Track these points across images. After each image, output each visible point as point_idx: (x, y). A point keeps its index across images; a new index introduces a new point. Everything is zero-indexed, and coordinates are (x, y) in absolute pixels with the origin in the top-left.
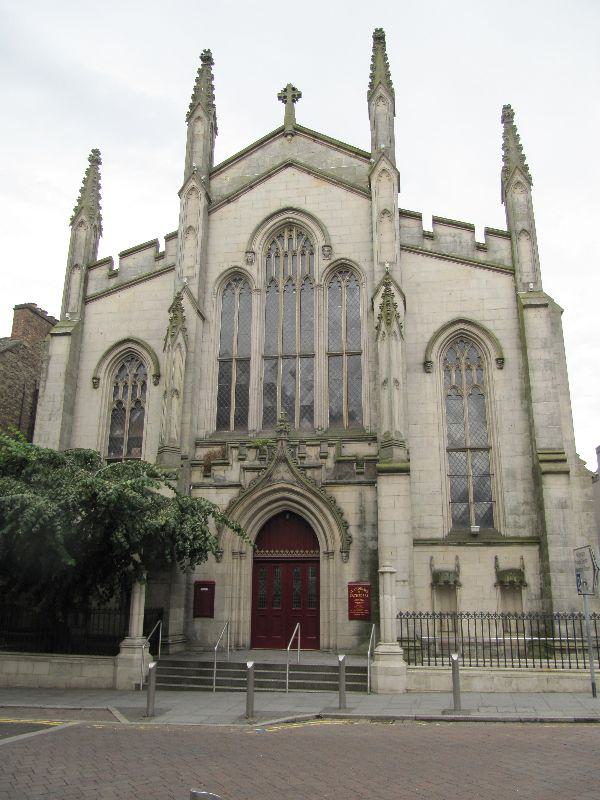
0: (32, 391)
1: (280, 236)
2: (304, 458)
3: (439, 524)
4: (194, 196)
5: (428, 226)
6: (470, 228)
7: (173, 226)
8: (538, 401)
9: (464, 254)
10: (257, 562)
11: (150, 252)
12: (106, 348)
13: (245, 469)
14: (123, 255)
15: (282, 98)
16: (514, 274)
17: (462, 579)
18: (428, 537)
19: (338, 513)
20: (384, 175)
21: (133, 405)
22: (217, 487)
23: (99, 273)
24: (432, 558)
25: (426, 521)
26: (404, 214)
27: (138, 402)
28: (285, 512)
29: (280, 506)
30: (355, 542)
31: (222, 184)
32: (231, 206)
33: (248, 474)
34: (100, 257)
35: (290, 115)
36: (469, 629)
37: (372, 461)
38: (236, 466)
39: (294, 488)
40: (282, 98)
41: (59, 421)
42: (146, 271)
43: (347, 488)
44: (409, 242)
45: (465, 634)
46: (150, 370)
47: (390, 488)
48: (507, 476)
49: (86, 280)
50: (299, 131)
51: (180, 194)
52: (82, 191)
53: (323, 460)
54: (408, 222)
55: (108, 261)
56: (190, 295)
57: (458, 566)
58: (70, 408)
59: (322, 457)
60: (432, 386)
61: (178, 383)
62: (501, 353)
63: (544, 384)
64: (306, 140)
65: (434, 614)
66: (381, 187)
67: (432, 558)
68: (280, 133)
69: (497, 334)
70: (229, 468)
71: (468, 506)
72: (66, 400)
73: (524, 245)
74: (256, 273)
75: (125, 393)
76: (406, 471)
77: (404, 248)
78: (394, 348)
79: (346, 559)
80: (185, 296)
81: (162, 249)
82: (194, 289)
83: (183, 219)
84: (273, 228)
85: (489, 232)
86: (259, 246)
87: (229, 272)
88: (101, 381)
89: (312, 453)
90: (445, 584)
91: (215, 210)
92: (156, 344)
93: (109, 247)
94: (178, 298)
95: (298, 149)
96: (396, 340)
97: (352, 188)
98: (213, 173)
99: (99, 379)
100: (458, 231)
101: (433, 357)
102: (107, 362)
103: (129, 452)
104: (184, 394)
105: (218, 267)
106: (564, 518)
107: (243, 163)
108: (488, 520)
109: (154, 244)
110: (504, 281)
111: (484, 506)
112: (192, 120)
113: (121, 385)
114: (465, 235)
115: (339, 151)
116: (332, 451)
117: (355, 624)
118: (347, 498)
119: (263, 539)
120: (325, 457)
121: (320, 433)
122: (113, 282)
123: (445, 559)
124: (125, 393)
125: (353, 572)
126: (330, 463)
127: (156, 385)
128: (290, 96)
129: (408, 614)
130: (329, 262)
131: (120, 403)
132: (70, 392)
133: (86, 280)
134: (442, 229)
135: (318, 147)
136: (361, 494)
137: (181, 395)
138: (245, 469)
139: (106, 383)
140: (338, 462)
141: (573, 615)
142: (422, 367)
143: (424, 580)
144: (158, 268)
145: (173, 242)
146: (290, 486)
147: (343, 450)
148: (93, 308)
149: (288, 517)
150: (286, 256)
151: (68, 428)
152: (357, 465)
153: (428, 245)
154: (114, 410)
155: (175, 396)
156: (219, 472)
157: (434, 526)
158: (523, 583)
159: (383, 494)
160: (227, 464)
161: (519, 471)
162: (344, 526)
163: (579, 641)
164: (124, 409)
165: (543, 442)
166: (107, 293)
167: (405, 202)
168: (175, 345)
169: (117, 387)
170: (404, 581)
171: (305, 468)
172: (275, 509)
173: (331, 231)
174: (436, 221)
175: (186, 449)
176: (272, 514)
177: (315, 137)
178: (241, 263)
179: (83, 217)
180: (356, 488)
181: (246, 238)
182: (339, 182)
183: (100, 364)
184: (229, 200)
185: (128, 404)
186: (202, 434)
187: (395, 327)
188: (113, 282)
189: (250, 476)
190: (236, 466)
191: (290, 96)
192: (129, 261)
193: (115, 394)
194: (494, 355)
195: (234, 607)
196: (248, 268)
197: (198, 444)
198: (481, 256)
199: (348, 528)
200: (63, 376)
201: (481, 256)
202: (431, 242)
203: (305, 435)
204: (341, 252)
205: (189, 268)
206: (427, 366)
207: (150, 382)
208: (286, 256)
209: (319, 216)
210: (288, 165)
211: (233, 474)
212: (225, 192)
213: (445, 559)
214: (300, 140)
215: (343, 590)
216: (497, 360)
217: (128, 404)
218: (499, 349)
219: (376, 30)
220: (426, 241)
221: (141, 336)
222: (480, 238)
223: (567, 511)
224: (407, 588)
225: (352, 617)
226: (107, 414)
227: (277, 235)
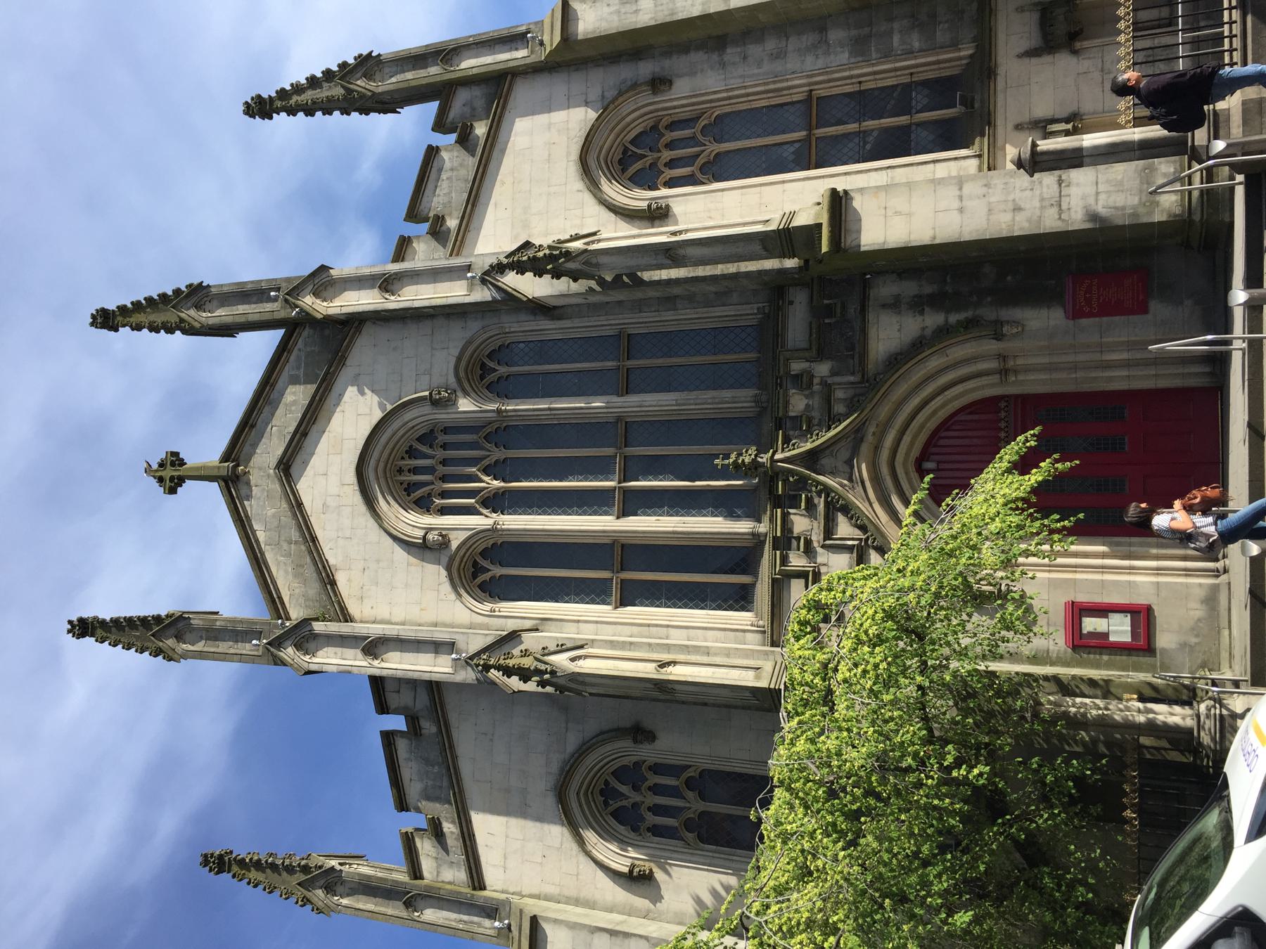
11: (402, 746)
19: (918, 347)
29: (907, 473)
32: (341, 579)
35: (203, 475)
53: (816, 381)
64: (383, 613)
71: (918, 125)
75: (656, 790)
109: (388, 738)
111: (919, 98)
113: (652, 819)
115: (276, 381)
117: (1154, 306)
124: (656, 789)
125: (1044, 312)
126: (823, 369)
131: (688, 825)
136: (884, 306)
145: (393, 700)
151: (419, 539)
159: (881, 240)
161: (854, 32)
163: (1231, 58)
164: (703, 814)
170: (1060, 182)
180: (871, 317)
184: (328, 580)
185: (695, 805)
194: (645, 98)
207: (648, 753)
212: (314, 588)
217: (695, 805)
219: (92, 324)
225: (1143, 310)
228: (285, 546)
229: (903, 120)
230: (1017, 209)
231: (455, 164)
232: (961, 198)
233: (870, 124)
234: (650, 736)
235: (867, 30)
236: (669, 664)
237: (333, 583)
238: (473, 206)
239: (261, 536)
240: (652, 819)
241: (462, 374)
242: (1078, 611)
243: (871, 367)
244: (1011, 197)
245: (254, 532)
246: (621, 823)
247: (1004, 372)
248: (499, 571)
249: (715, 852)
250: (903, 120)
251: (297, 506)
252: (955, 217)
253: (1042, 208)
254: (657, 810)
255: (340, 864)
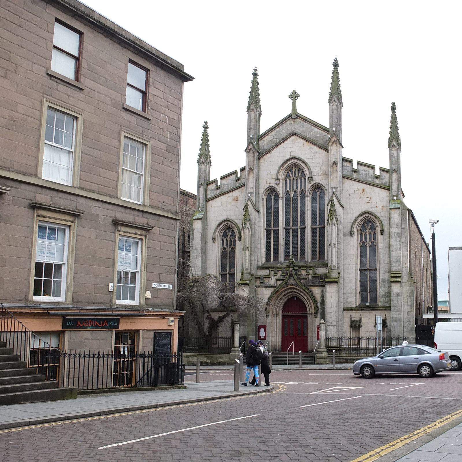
0: (182, 233)
1: (291, 170)
2: (300, 275)
3: (354, 300)
4: (251, 152)
5: (355, 166)
6: (373, 167)
7: (243, 165)
8: (392, 251)
9: (370, 180)
10: (283, 317)
11: (234, 177)
12: (217, 224)
13: (277, 280)
14: (222, 178)
15: (290, 97)
16: (389, 190)
17: (362, 324)
18: (350, 307)
19: (314, 298)
20: (335, 143)
21: (230, 249)
22: (266, 287)
23: (212, 187)
24: (351, 315)
25: (349, 300)
26: (344, 160)
27: (232, 248)
28: (294, 297)
30: (320, 309)
31: (265, 143)
32: (268, 155)
33: (278, 281)
34: (211, 179)
36: (364, 344)
37: (326, 276)
38: (273, 278)
39: (296, 288)
40: (290, 97)
41: (200, 259)
42: (233, 186)
43: (317, 288)
44: (346, 173)
45: (363, 345)
46: (237, 235)
47: (331, 291)
48: (382, 281)
49: (206, 191)
50: (299, 116)
51: (246, 151)
52: (201, 145)
54: (346, 164)
55: (215, 181)
56: (252, 202)
57: (361, 319)
58: (204, 252)
59: (307, 275)
60: (354, 243)
61: (248, 245)
62: (383, 228)
63: (396, 243)
65: (351, 338)
66: (333, 148)
67: (351, 315)
68: (289, 117)
69: (382, 219)
70: (271, 279)
72: (202, 249)
73: (395, 176)
74: (281, 190)
75: (231, 241)
76: (336, 282)
77: (344, 177)
78: (334, 229)
79: (316, 316)
80: (249, 203)
81: (239, 175)
82: (254, 199)
83: (248, 162)
84: (287, 167)
85: (382, 170)
86: (281, 176)
87: (269, 188)
88: (216, 239)
89: (303, 273)
90: (356, 326)
91: (261, 157)
92: (239, 222)
93: (215, 174)
94: (246, 206)
95: (297, 126)
96: (335, 226)
97: (321, 147)
98: (260, 137)
99: (215, 238)
100: (367, 169)
101: (355, 229)
102: (217, 233)
103: (230, 270)
104: (252, 249)
105: (264, 186)
106: (398, 300)
107: (273, 133)
108: (374, 299)
109: (235, 173)
110: (384, 194)
112: (250, 111)
113: (225, 240)
114: (371, 171)
116: (311, 272)
118: (317, 291)
119: (286, 307)
120: (308, 275)
121: (307, 263)
122: (218, 192)
123: (356, 316)
126: (310, 277)
127: (239, 241)
128: (294, 96)
129: (337, 338)
130: (311, 184)
131: (225, 248)
132: (218, 322)
133: (206, 191)
134: (362, 168)
135: (307, 125)
137: (250, 248)
138: (277, 280)
139: (218, 240)
140: (313, 277)
141: (399, 338)
142: (349, 233)
143: (347, 324)
144: (238, 185)
146: (294, 287)
147: (316, 271)
148: (210, 203)
149: (295, 299)
150: (293, 179)
152: (321, 278)
153: (355, 175)
154: (222, 251)
155: (247, 250)
156: (267, 281)
157: (352, 302)
158: (200, 363)
160: (270, 278)
161: (387, 279)
162: (316, 303)
165: (394, 268)
166: (216, 197)
167: (346, 153)
168: (246, 228)
169: (223, 241)
170: (335, 325)
171: (301, 279)
172: (290, 296)
173: (312, 169)
174: (359, 164)
175: (254, 272)
176: (288, 298)
177: (306, 120)
178: (273, 185)
179: (203, 159)
180: (320, 287)
181: (275, 172)
182: (316, 144)
183: (215, 232)
185: (228, 249)
186: (259, 264)
187: (334, 221)
188: (218, 192)
189: (279, 283)
190: (273, 278)
191: (294, 96)
192: (224, 181)
193: (223, 244)
195: (274, 336)
196: (276, 187)
197: (259, 268)
198: (377, 181)
199: (317, 304)
200: (200, 239)
201: (377, 181)
202: (356, 174)
203: (301, 264)
204: (317, 179)
205: (251, 188)
206: (351, 234)
207: (237, 239)
208: (293, 179)
209: (307, 161)
210: (294, 134)
211: (272, 282)
212: (266, 147)
213: (356, 316)
214: (299, 121)
215: (315, 328)
216: (380, 231)
217: (228, 249)
218: (382, 225)
220: (354, 173)
221: (232, 218)
222: (378, 172)
223: (399, 297)
224: (335, 328)
226: (219, 254)
227: (290, 169)
228: (276, 137)
229: (368, 291)
230: (330, 317)
231: (369, 175)
232: (334, 307)
233: (368, 283)
234: (240, 240)
235: (387, 282)
236: (248, 249)
237: (268, 153)
238: (359, 182)
239: (278, 129)
240: (225, 240)
241: (316, 184)
242: (265, 327)
243: (310, 288)
244: (333, 317)
245: (279, 127)
246: (224, 233)
247: (309, 314)
248: (273, 197)
249: (220, 255)
250: (368, 291)
251: (285, 140)
252: (330, 306)
253: (330, 322)
254: (227, 241)
255: (208, 163)
